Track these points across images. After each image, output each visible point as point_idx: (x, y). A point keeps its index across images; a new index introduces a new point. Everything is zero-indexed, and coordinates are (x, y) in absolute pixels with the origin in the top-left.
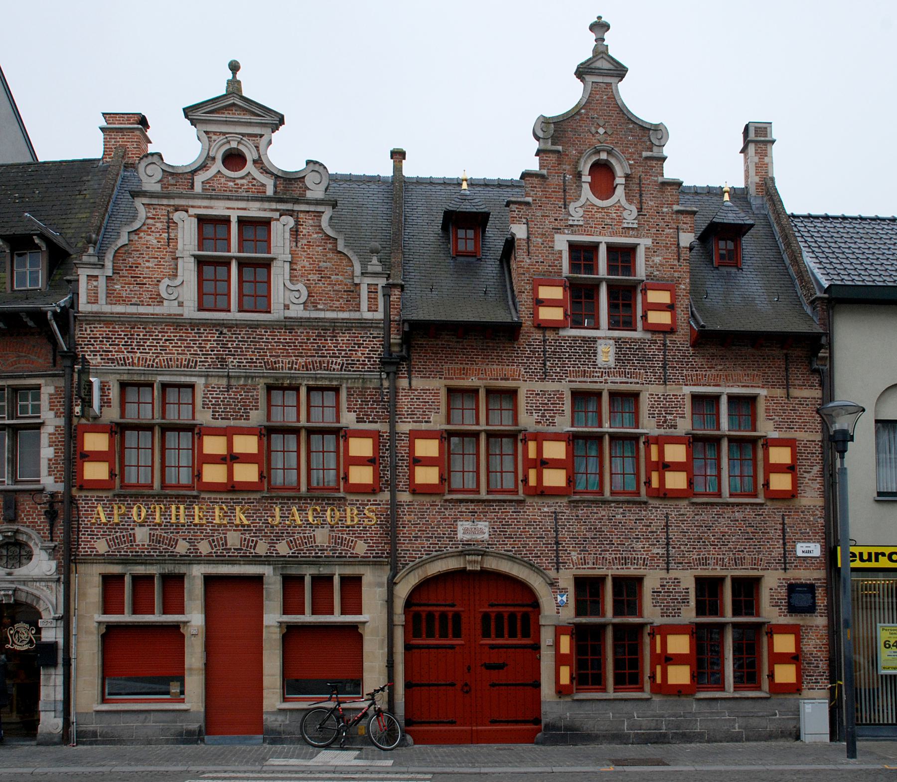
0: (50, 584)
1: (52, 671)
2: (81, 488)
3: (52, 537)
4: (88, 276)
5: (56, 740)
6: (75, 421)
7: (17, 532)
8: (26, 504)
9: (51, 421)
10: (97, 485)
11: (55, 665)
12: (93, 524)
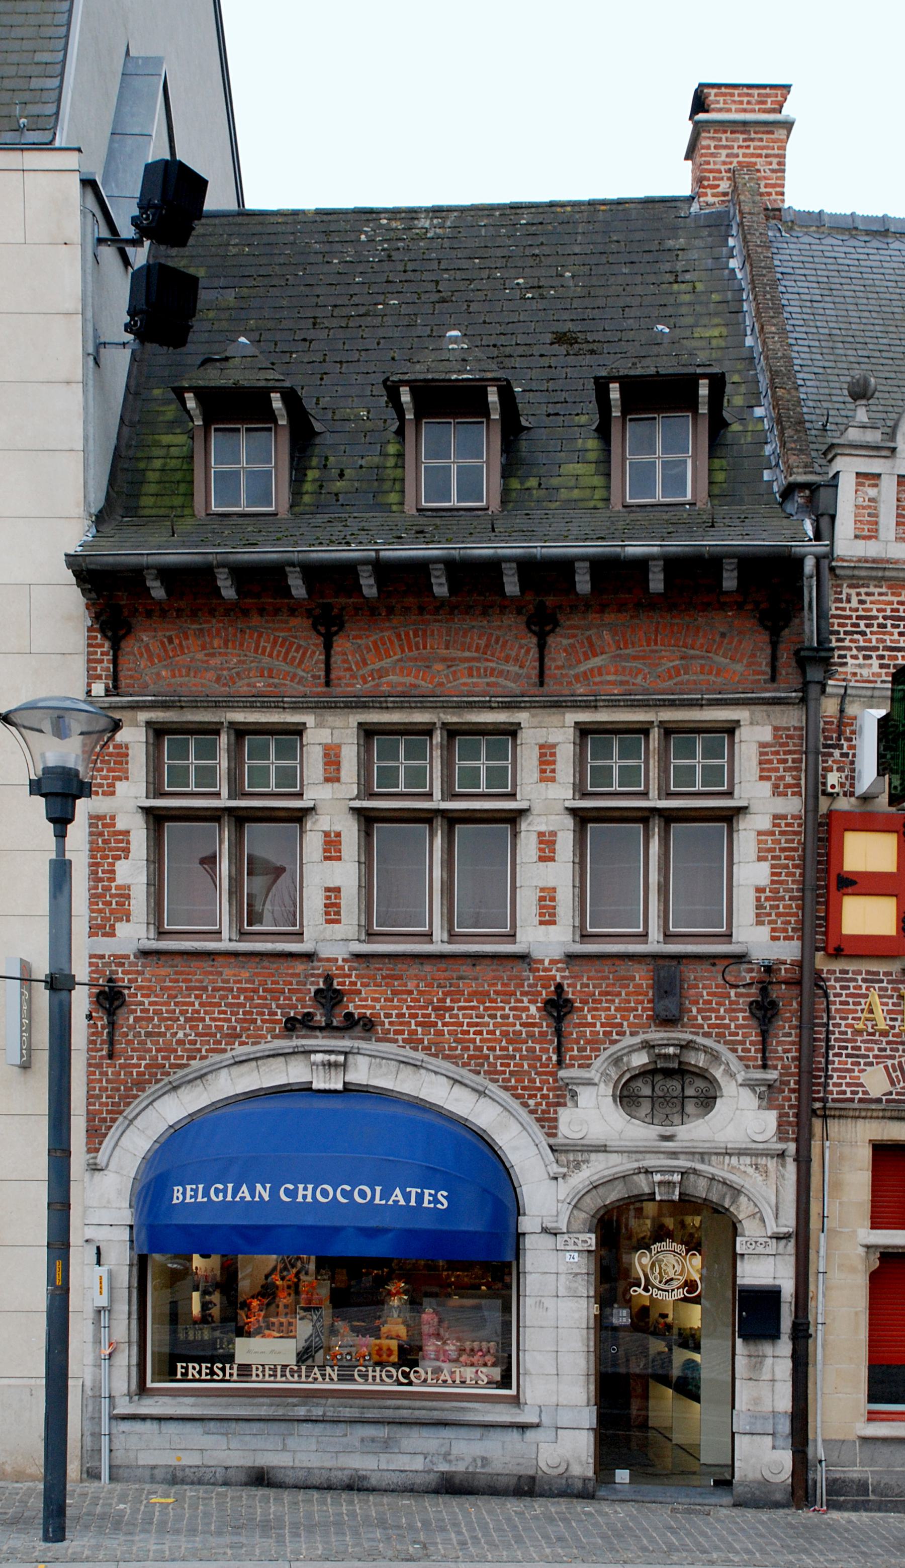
0: (762, 1161)
1: (767, 1348)
2: (838, 953)
3: (764, 1058)
4: (858, 474)
5: (779, 1496)
6: (824, 805)
7: (687, 1046)
8: (703, 986)
9: (764, 802)
10: (869, 948)
11: (774, 1336)
12: (859, 1032)
